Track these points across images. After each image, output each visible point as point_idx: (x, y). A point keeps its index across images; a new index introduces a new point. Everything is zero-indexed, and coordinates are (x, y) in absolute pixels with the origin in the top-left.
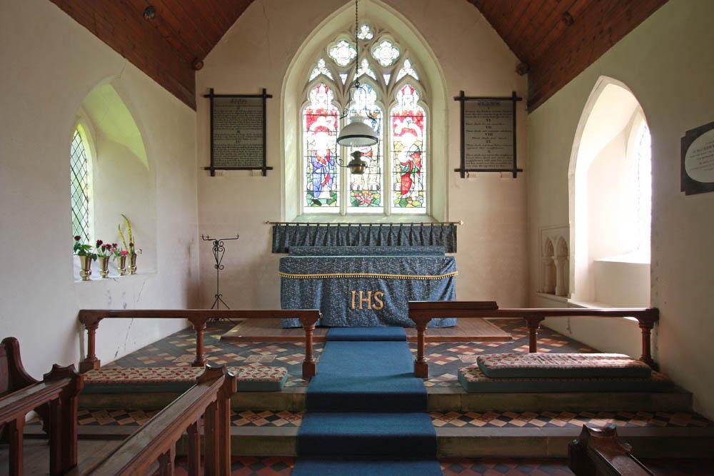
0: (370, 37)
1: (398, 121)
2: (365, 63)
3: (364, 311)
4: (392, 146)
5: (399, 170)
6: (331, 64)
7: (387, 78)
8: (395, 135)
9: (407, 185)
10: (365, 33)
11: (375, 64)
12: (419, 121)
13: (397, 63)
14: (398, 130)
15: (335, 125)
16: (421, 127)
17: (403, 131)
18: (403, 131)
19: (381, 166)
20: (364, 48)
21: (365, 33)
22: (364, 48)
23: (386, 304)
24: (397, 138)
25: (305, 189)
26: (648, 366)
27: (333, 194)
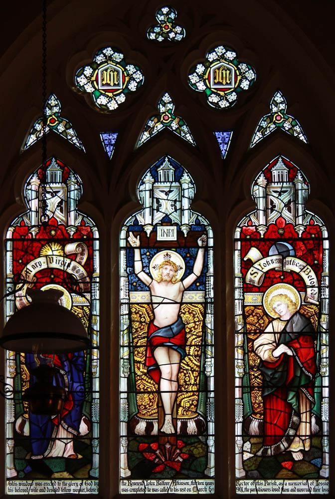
0: (177, 34)
1: (254, 254)
2: (167, 104)
3: (87, 352)
4: (239, 319)
5: (257, 382)
6: (80, 108)
7: (224, 140)
8: (248, 288)
9: (278, 421)
10: (166, 27)
11: (192, 105)
12: (310, 251)
13: (251, 104)
14: (255, 276)
15: (89, 266)
16: (318, 269)
17: (270, 278)
18: (270, 278)
19: (210, 370)
20: (166, 69)
21: (166, 27)
22: (166, 69)
23: (86, 360)
24: (252, 298)
25: (9, 433)
26: (5, 326)
27: (81, 444)
